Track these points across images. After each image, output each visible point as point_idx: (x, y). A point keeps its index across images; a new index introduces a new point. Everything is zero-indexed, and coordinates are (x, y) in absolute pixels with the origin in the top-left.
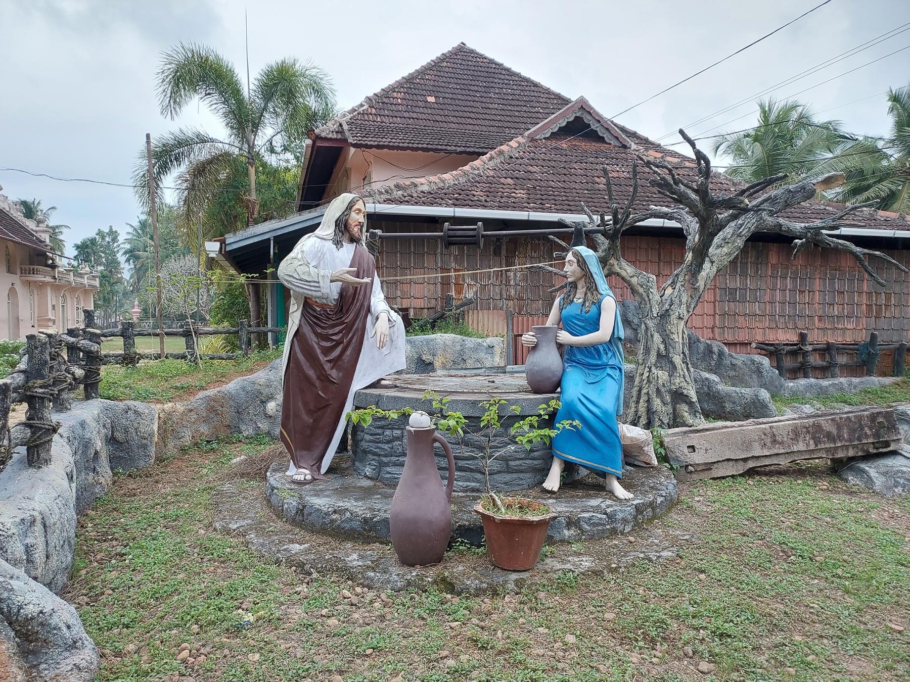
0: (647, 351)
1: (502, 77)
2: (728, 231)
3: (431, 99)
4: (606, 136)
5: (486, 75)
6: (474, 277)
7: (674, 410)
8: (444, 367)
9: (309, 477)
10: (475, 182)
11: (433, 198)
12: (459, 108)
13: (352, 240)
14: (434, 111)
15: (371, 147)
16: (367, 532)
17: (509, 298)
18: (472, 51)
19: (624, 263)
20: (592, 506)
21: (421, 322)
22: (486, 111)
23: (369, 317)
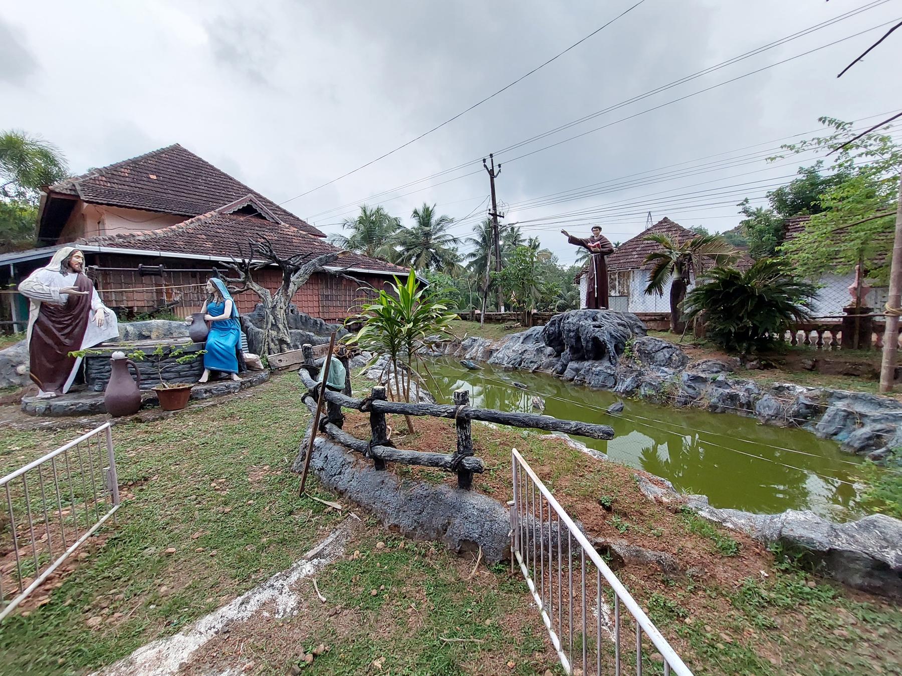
3: (154, 177)
6: (179, 289)
11: (144, 244)
13: (75, 271)
15: (102, 204)
16: (93, 410)
18: (185, 151)
20: (221, 385)
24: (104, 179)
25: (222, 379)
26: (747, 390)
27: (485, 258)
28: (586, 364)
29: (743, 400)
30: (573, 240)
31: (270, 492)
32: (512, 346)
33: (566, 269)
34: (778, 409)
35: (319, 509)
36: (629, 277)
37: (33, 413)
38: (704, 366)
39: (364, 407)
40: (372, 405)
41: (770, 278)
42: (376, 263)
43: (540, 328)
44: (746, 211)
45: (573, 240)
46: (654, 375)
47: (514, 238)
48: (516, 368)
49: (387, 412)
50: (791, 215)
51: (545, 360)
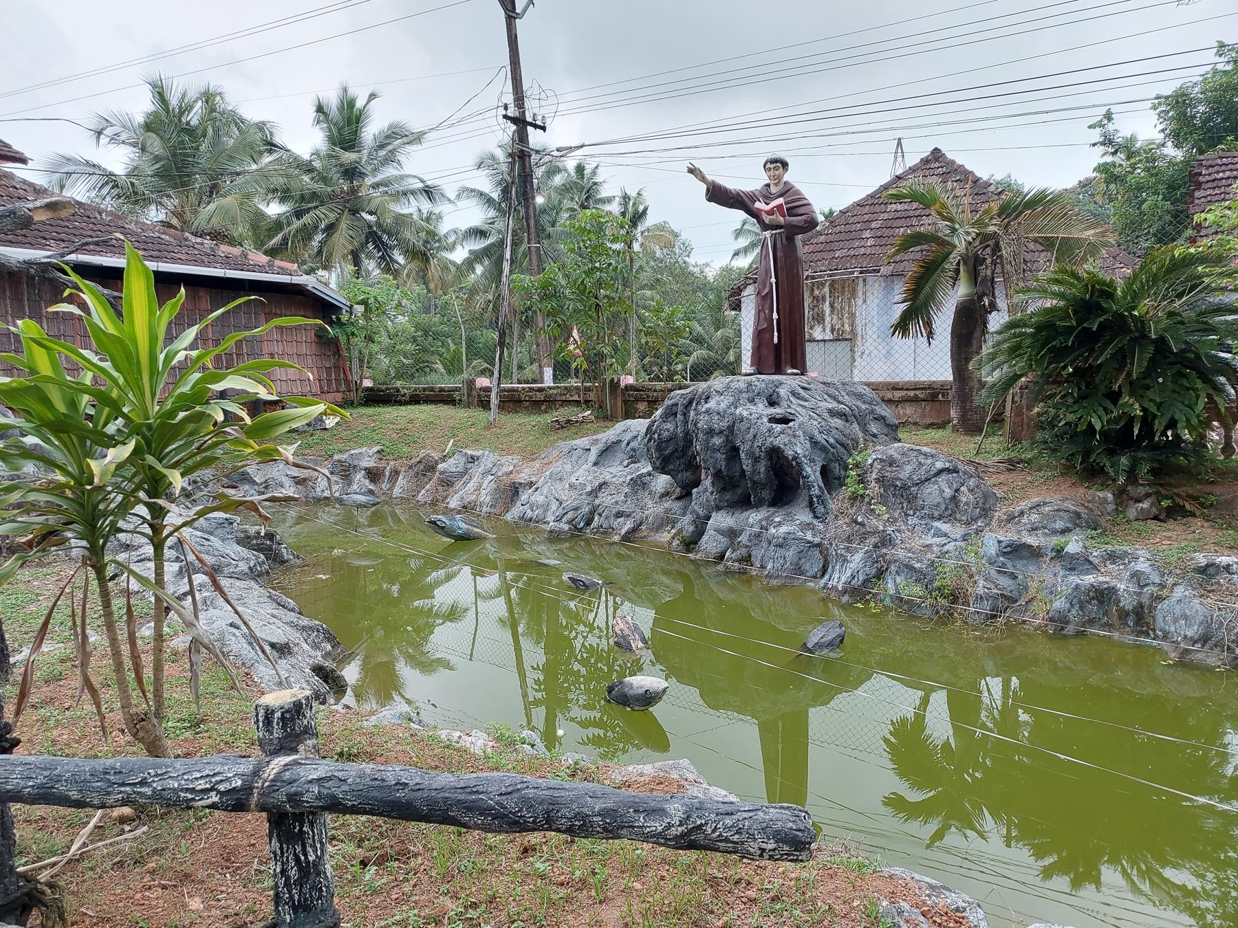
26: (1136, 575)
28: (754, 517)
29: (1127, 602)
30: (718, 195)
32: (574, 471)
33: (711, 274)
34: (1207, 623)
36: (853, 293)
38: (1034, 517)
41: (1180, 296)
42: (182, 242)
44: (1107, 141)
45: (718, 195)
46: (917, 543)
47: (584, 189)
48: (580, 531)
50: (1201, 152)
51: (653, 509)
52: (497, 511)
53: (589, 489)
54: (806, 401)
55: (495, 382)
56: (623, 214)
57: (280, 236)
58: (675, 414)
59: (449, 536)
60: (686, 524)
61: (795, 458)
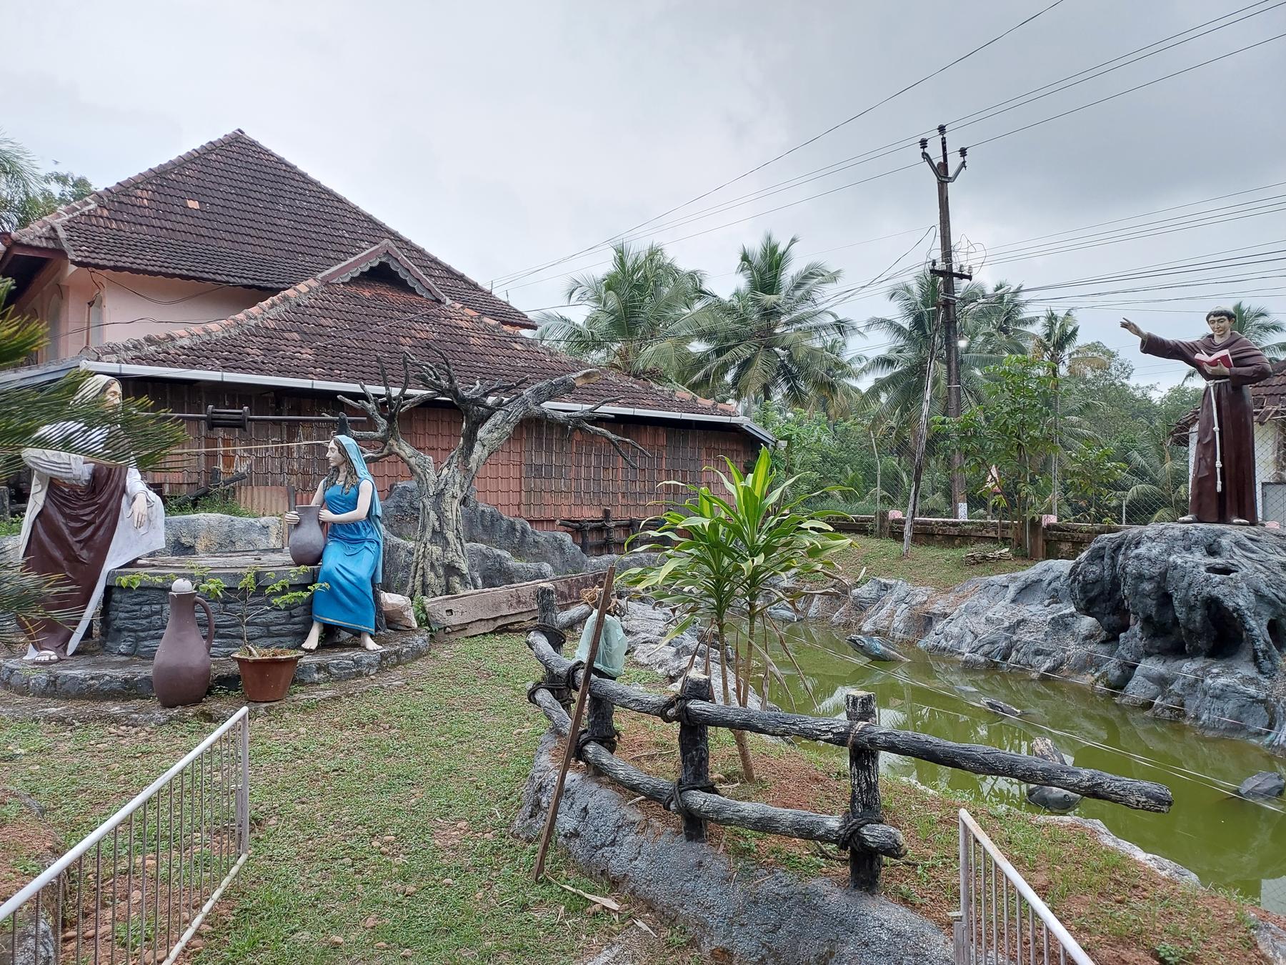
0: (424, 527)
1: (295, 184)
2: (498, 416)
3: (193, 204)
4: (417, 287)
5: (273, 178)
7: (448, 583)
8: (208, 550)
9: (55, 657)
10: (255, 332)
11: (195, 356)
12: (234, 221)
14: (197, 222)
15: (104, 267)
16: (128, 690)
17: (291, 473)
18: (253, 144)
19: (403, 444)
21: (178, 500)
22: (271, 228)
23: (124, 499)
24: (106, 213)
25: (343, 646)
27: (918, 370)
28: (1188, 668)
31: (478, 868)
32: (986, 606)
33: (1156, 397)
35: (578, 905)
37: (23, 690)
39: (671, 712)
40: (687, 710)
43: (1062, 566)
48: (996, 665)
49: (716, 724)
51: (1074, 650)
52: (910, 638)
53: (1006, 624)
54: (1253, 552)
55: (909, 515)
56: (1048, 336)
57: (702, 372)
58: (1102, 558)
59: (867, 655)
60: (1112, 668)
61: (1236, 610)
